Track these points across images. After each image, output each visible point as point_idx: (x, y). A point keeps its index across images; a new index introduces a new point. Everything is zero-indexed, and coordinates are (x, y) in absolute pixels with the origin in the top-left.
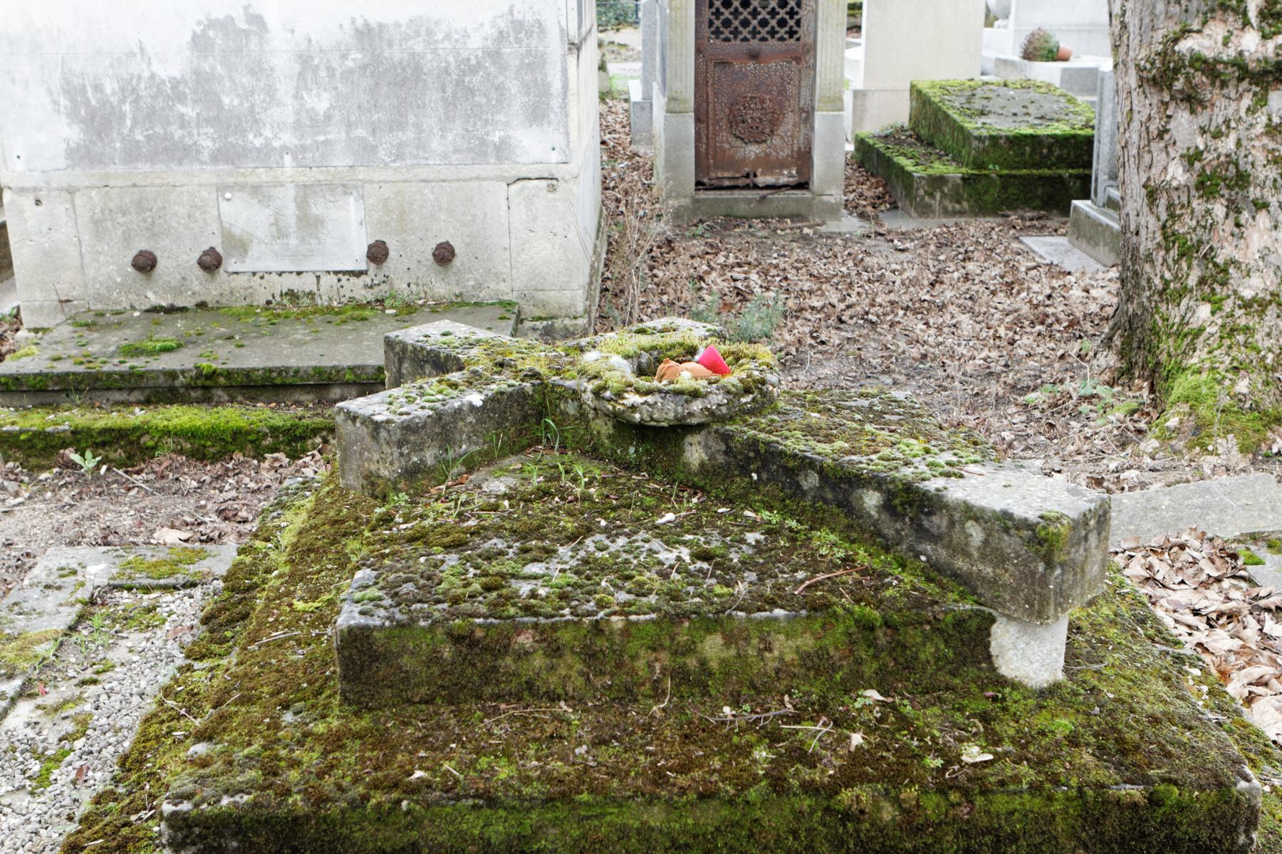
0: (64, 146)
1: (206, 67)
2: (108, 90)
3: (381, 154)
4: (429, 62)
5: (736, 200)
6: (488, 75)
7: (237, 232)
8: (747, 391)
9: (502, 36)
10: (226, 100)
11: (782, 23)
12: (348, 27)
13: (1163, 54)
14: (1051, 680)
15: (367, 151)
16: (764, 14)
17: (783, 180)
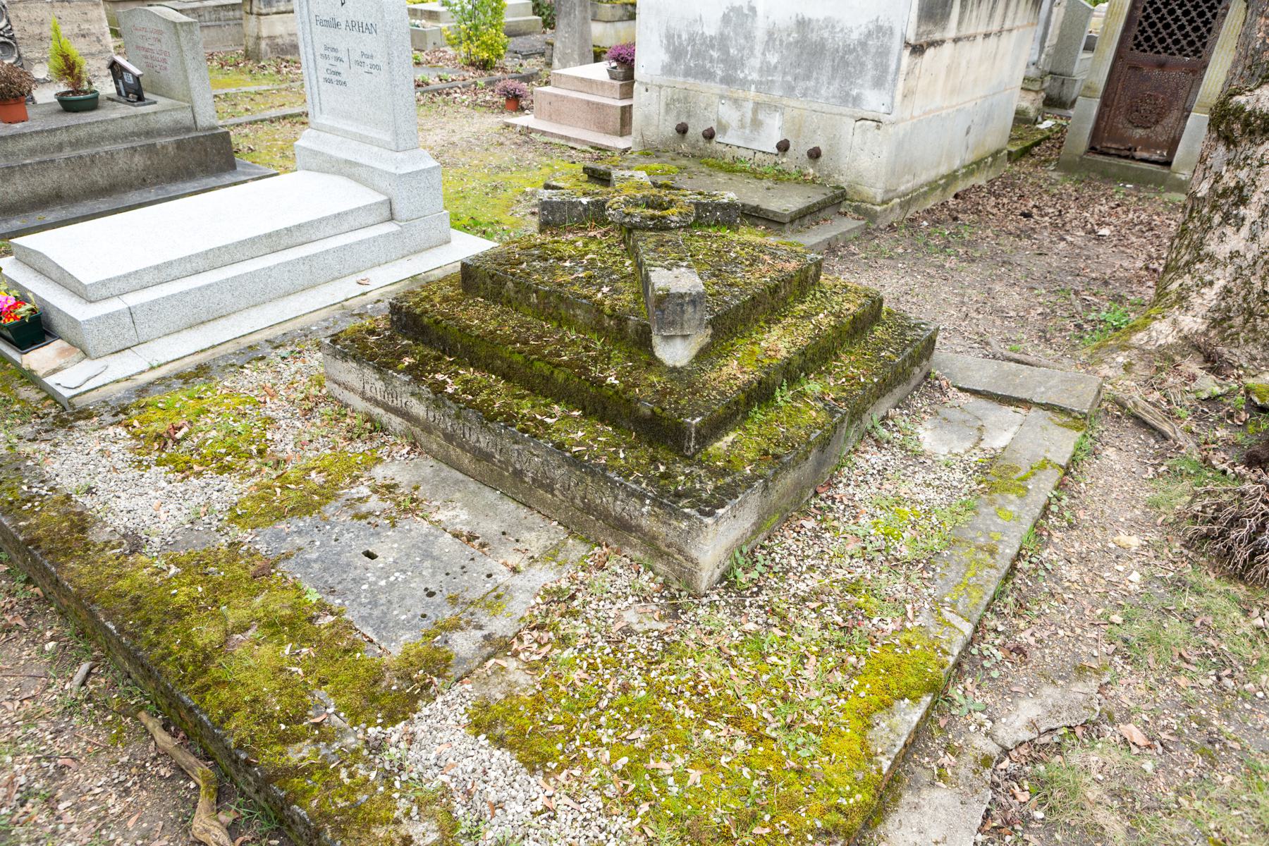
3: (797, 92)
4: (830, 44)
5: (1110, 164)
9: (869, 34)
17: (1155, 157)
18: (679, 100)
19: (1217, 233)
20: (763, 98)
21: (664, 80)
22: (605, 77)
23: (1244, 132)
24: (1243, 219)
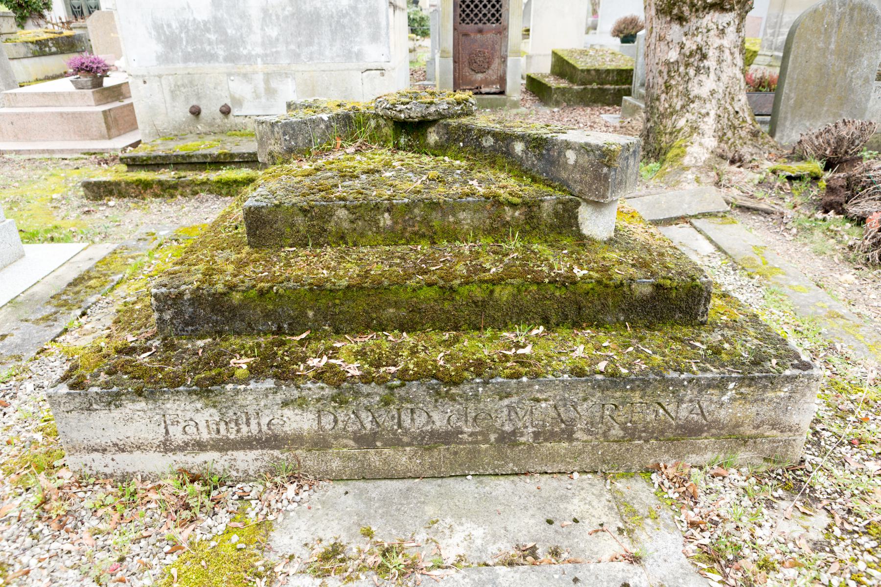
0: (155, 54)
1: (219, 15)
2: (174, 27)
3: (303, 57)
6: (351, 18)
7: (237, 96)
15: (296, 56)
17: (493, 90)
18: (184, 86)
19: (696, 81)
20: (271, 68)
22: (71, 88)
23: (691, 11)
24: (709, 68)
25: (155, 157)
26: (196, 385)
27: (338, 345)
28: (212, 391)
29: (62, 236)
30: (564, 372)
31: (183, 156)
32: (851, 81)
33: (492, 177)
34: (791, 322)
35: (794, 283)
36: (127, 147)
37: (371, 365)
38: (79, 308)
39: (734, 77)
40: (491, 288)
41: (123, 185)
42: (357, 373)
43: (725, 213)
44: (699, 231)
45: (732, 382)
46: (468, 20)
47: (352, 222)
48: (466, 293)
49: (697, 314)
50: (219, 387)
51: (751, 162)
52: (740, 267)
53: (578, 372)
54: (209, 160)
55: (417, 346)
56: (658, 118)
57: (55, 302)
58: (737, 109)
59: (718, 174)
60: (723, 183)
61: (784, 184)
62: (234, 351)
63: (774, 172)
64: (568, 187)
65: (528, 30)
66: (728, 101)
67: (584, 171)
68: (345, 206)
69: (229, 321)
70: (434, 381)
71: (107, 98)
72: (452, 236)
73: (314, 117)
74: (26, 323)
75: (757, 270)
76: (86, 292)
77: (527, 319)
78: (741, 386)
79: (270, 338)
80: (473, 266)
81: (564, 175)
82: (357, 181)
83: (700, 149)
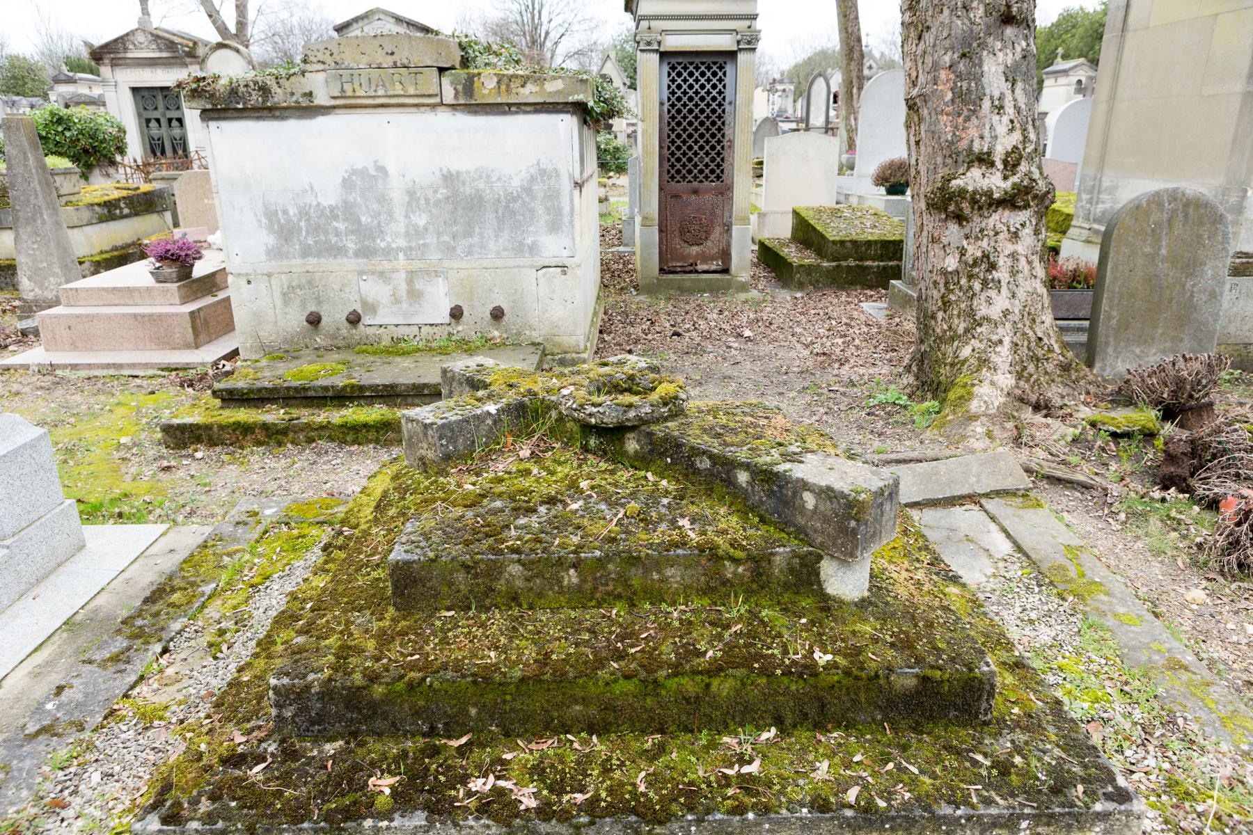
1: (351, 199)
2: (291, 213)
4: (488, 195)
7: (370, 300)
8: (665, 404)
10: (363, 219)
11: (712, 171)
12: (437, 173)
13: (941, 189)
14: (860, 596)
16: (701, 166)
17: (713, 268)
18: (300, 287)
20: (416, 265)
21: (274, 266)
22: (150, 281)
23: (973, 208)
24: (999, 282)
25: (260, 390)
26: (325, 820)
27: (508, 756)
28: (344, 830)
29: (134, 511)
30: (803, 806)
31: (296, 389)
32: (1192, 296)
33: (708, 512)
34: (1116, 676)
35: (1121, 610)
36: (220, 359)
37: (551, 791)
38: (160, 640)
39: (1035, 292)
40: (707, 681)
41: (215, 429)
42: (533, 803)
43: (1027, 490)
44: (993, 519)
45: (1025, 820)
46: (678, 178)
47: (528, 580)
48: (674, 686)
49: (977, 713)
50: (354, 824)
51: (1061, 408)
52: (1047, 581)
53: (820, 805)
54: (330, 394)
55: (609, 759)
56: (934, 341)
57: (127, 630)
58: (1040, 335)
59: (1016, 427)
60: (1024, 440)
61: (1107, 444)
62: (373, 764)
63: (1093, 425)
64: (807, 535)
65: (761, 163)
66: (1028, 323)
67: (826, 520)
68: (519, 561)
69: (368, 719)
70: (633, 818)
71: (195, 293)
72: (657, 596)
73: (479, 412)
74: (89, 667)
75: (1069, 587)
76: (168, 614)
77: (754, 719)
78: (1037, 825)
79: (421, 742)
80: (683, 646)
81: (801, 521)
82: (534, 518)
83: (992, 390)
